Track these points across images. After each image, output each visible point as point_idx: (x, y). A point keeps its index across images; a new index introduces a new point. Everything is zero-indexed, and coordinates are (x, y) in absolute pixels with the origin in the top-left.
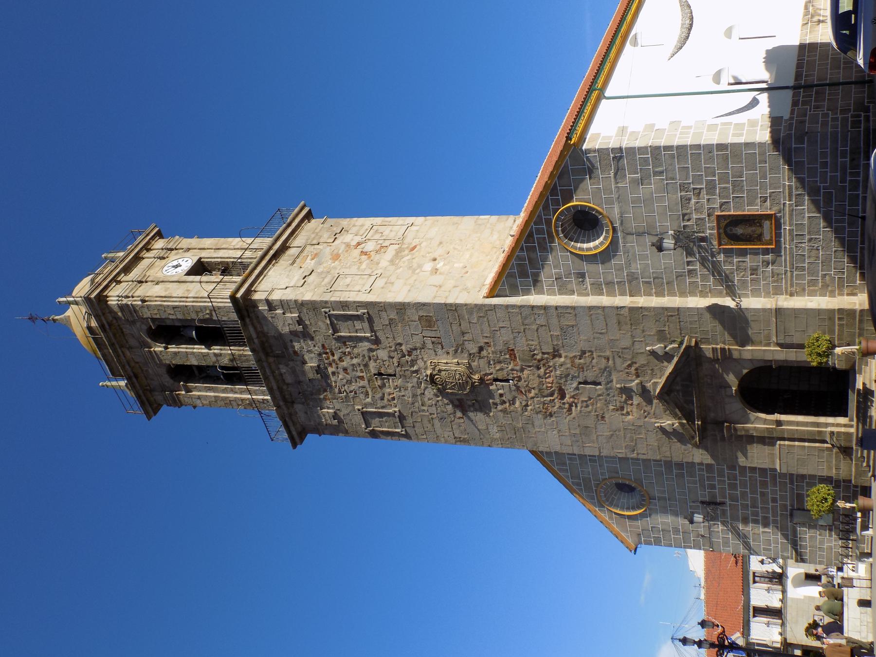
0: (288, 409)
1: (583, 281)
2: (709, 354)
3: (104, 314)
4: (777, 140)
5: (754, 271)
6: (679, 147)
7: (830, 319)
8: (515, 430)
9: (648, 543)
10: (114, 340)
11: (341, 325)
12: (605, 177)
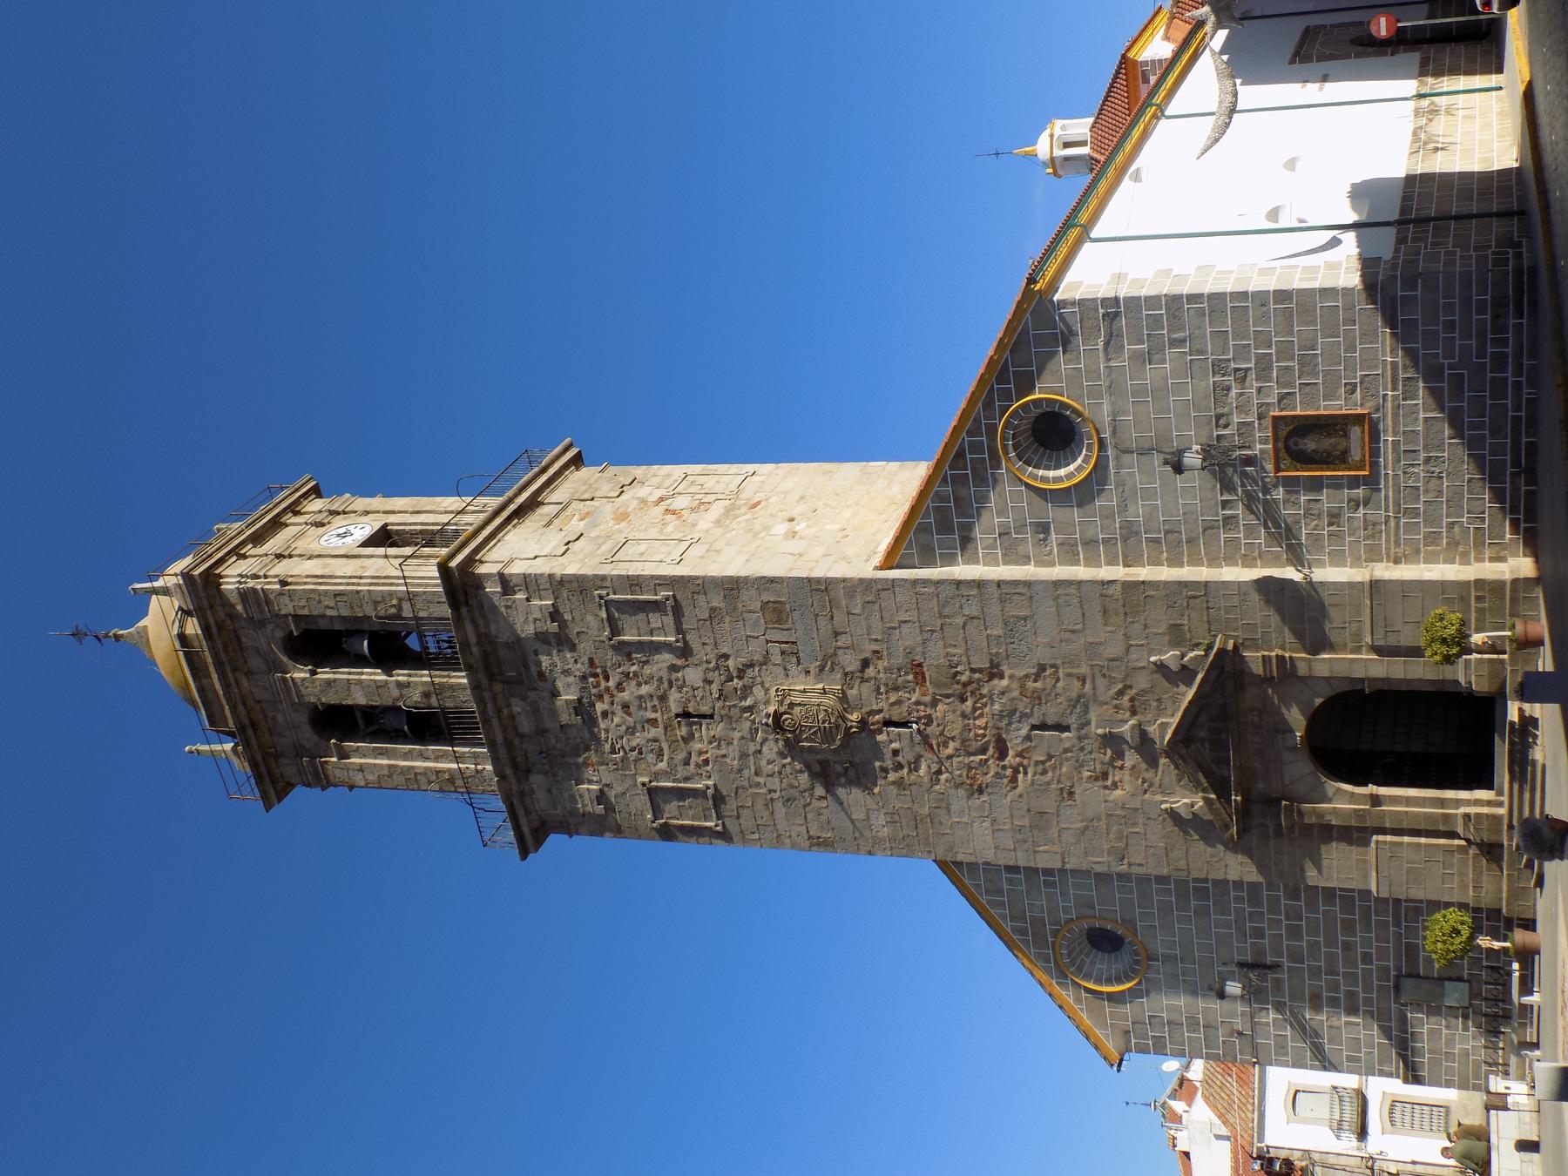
0: (519, 782)
1: (1045, 539)
2: (1257, 669)
3: (212, 607)
4: (1371, 285)
5: (1334, 517)
6: (1212, 296)
7: (1462, 599)
8: (916, 821)
9: (1142, 1050)
10: (223, 656)
11: (626, 621)
12: (1088, 347)
